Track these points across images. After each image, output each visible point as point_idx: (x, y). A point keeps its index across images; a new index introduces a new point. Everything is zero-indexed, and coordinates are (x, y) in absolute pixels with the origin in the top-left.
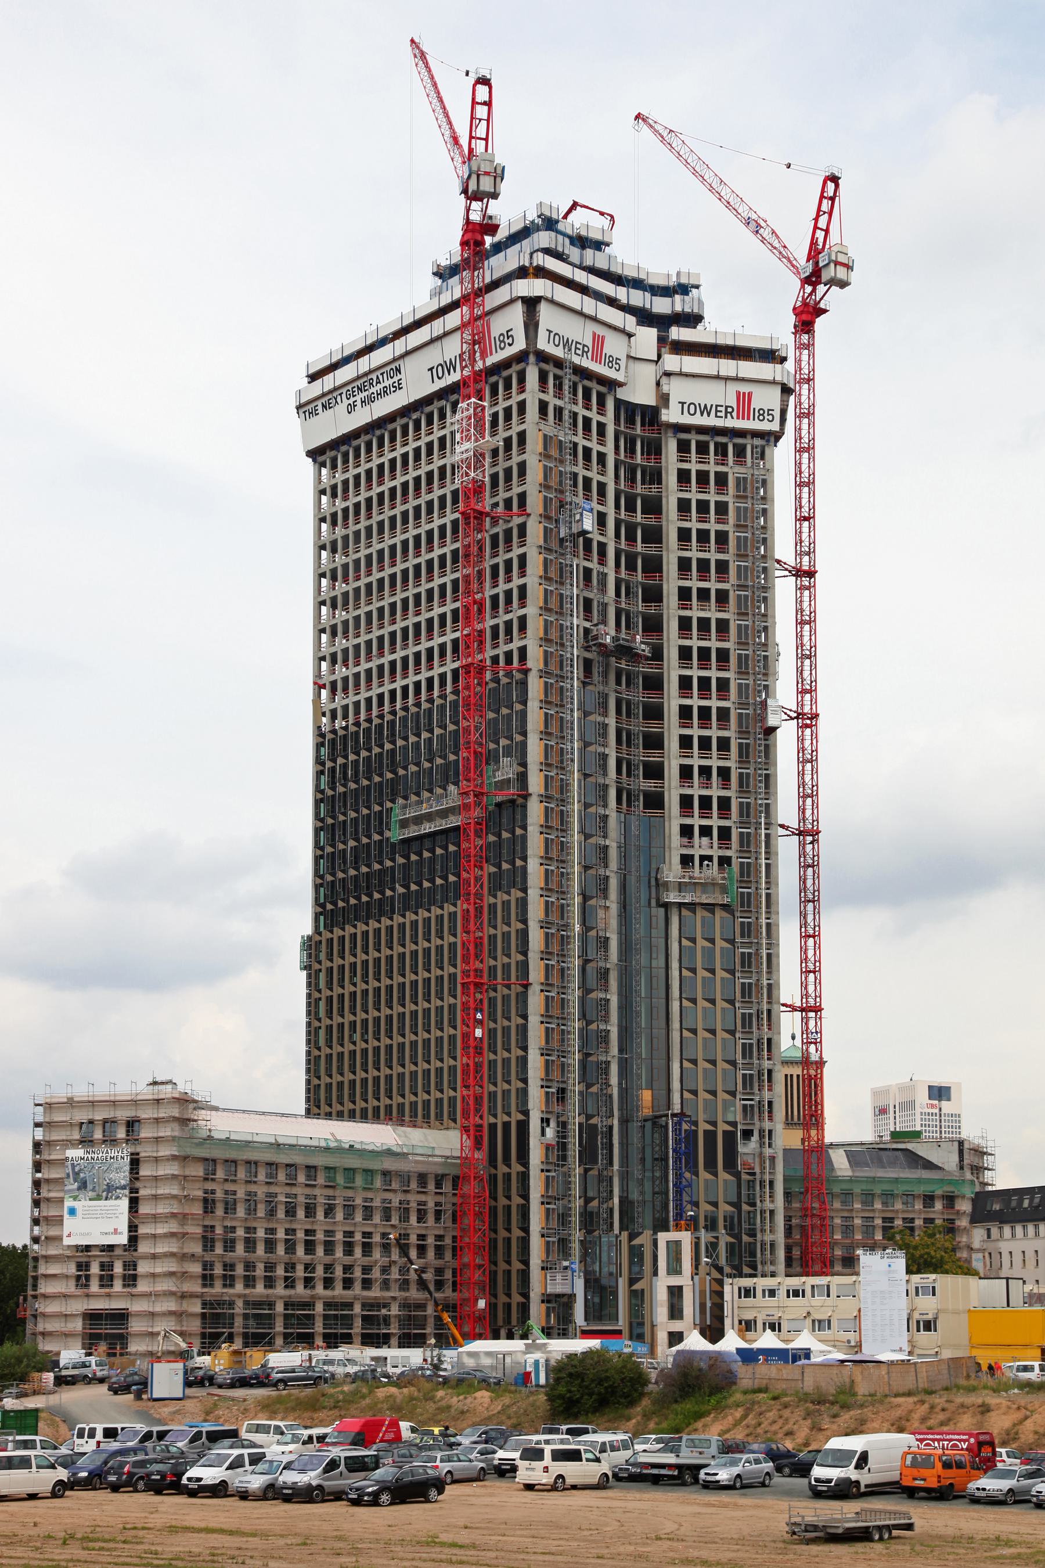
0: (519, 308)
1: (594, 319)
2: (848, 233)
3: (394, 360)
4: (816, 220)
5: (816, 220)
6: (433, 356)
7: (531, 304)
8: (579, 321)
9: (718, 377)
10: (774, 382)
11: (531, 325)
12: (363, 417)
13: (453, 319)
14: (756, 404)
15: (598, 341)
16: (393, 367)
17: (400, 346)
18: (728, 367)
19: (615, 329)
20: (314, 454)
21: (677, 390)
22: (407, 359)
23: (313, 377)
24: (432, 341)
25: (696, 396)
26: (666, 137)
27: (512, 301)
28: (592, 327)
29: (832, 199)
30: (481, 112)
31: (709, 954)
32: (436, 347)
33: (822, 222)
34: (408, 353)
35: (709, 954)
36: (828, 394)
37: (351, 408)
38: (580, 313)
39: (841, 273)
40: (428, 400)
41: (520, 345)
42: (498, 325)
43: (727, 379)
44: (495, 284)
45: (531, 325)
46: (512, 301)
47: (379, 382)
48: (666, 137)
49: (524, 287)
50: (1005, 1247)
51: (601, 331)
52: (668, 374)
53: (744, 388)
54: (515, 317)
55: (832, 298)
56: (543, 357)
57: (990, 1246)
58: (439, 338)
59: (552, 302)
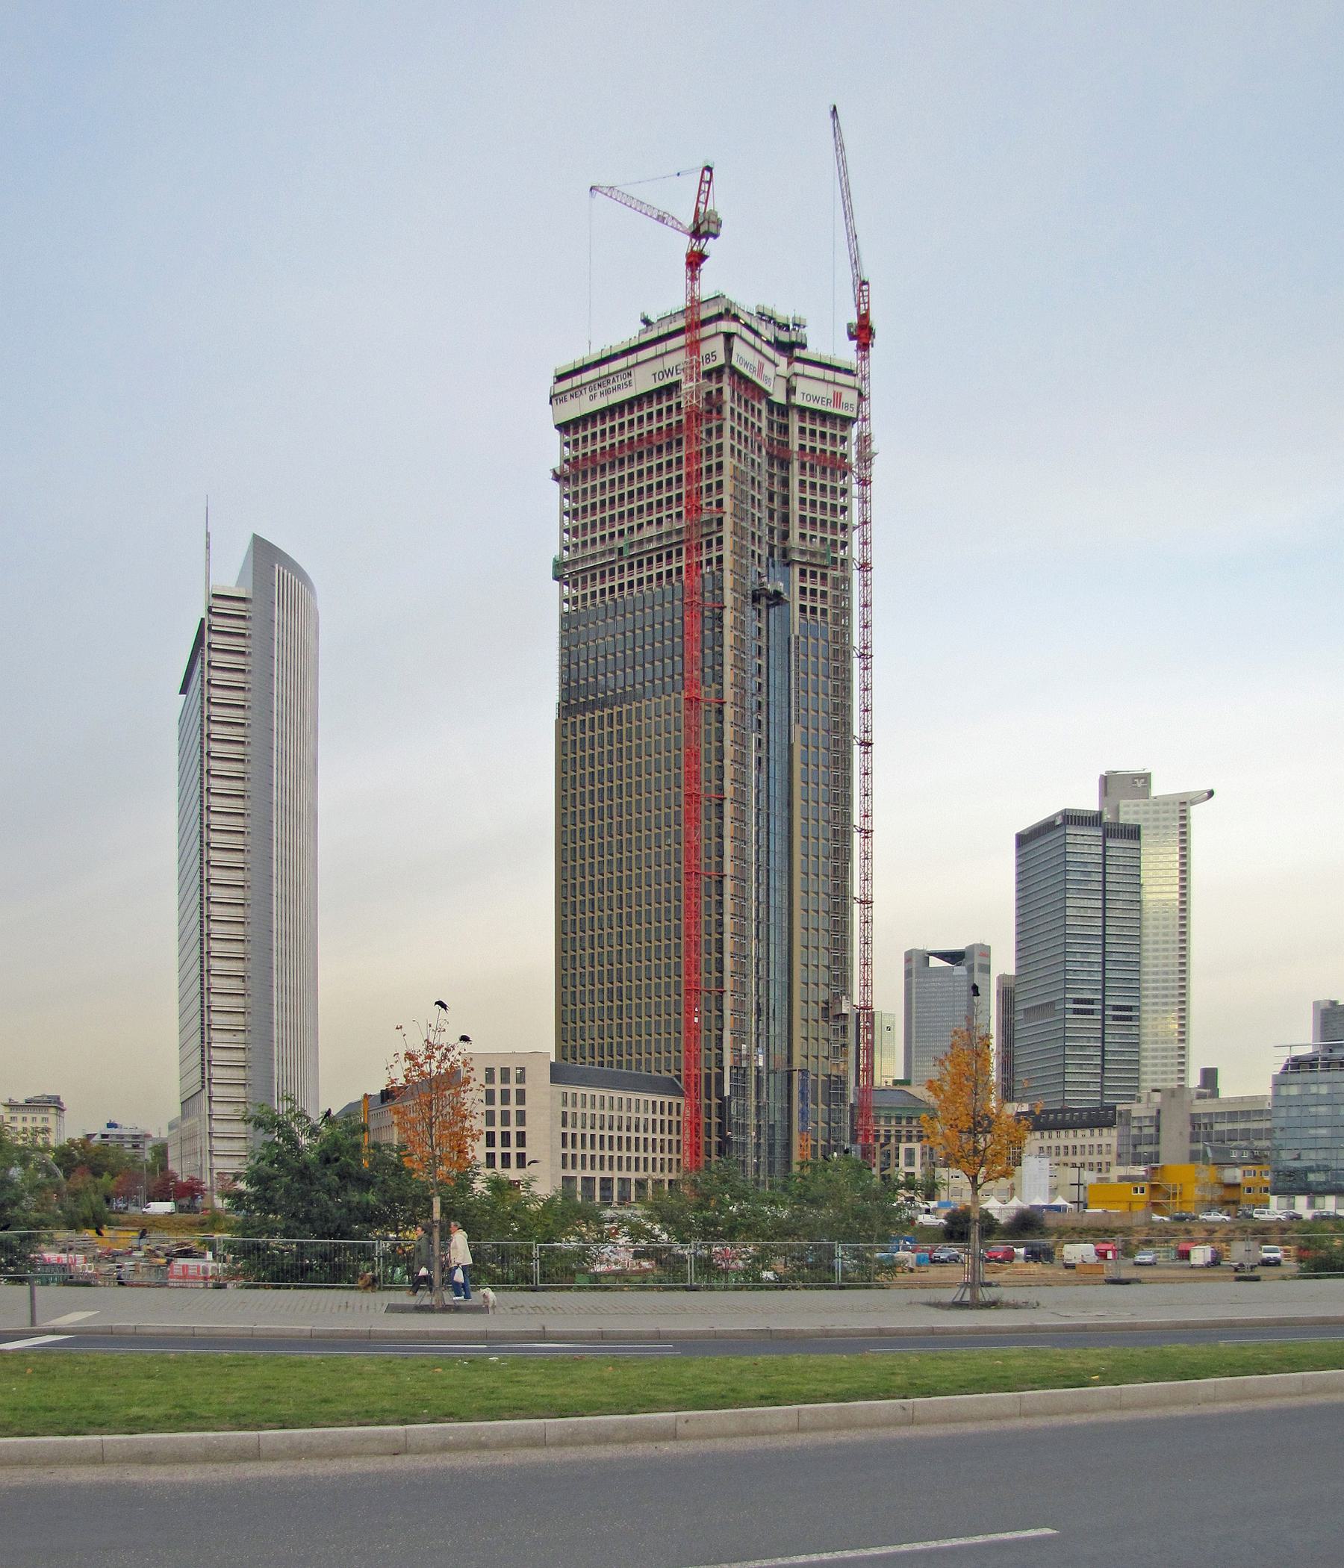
0: (721, 338)
1: (834, 383)
2: (719, 204)
3: (628, 368)
6: (657, 366)
7: (729, 337)
8: (824, 385)
9: (823, 380)
10: (854, 388)
11: (729, 351)
13: (680, 341)
14: (844, 399)
15: (761, 366)
16: (628, 370)
17: (631, 359)
18: (829, 375)
19: (849, 387)
20: (563, 427)
21: (801, 385)
23: (560, 378)
24: (657, 357)
25: (811, 392)
27: (717, 334)
28: (832, 388)
29: (709, 183)
31: (816, 665)
32: (659, 361)
33: (702, 198)
34: (638, 364)
35: (816, 665)
36: (876, 389)
37: (593, 397)
38: (823, 380)
39: (713, 229)
40: (648, 396)
41: (721, 360)
42: (705, 349)
43: (828, 382)
44: (705, 323)
45: (729, 351)
46: (717, 334)
49: (725, 326)
52: (796, 375)
53: (838, 389)
54: (719, 344)
55: (710, 246)
56: (734, 371)
58: (662, 355)
59: (740, 337)
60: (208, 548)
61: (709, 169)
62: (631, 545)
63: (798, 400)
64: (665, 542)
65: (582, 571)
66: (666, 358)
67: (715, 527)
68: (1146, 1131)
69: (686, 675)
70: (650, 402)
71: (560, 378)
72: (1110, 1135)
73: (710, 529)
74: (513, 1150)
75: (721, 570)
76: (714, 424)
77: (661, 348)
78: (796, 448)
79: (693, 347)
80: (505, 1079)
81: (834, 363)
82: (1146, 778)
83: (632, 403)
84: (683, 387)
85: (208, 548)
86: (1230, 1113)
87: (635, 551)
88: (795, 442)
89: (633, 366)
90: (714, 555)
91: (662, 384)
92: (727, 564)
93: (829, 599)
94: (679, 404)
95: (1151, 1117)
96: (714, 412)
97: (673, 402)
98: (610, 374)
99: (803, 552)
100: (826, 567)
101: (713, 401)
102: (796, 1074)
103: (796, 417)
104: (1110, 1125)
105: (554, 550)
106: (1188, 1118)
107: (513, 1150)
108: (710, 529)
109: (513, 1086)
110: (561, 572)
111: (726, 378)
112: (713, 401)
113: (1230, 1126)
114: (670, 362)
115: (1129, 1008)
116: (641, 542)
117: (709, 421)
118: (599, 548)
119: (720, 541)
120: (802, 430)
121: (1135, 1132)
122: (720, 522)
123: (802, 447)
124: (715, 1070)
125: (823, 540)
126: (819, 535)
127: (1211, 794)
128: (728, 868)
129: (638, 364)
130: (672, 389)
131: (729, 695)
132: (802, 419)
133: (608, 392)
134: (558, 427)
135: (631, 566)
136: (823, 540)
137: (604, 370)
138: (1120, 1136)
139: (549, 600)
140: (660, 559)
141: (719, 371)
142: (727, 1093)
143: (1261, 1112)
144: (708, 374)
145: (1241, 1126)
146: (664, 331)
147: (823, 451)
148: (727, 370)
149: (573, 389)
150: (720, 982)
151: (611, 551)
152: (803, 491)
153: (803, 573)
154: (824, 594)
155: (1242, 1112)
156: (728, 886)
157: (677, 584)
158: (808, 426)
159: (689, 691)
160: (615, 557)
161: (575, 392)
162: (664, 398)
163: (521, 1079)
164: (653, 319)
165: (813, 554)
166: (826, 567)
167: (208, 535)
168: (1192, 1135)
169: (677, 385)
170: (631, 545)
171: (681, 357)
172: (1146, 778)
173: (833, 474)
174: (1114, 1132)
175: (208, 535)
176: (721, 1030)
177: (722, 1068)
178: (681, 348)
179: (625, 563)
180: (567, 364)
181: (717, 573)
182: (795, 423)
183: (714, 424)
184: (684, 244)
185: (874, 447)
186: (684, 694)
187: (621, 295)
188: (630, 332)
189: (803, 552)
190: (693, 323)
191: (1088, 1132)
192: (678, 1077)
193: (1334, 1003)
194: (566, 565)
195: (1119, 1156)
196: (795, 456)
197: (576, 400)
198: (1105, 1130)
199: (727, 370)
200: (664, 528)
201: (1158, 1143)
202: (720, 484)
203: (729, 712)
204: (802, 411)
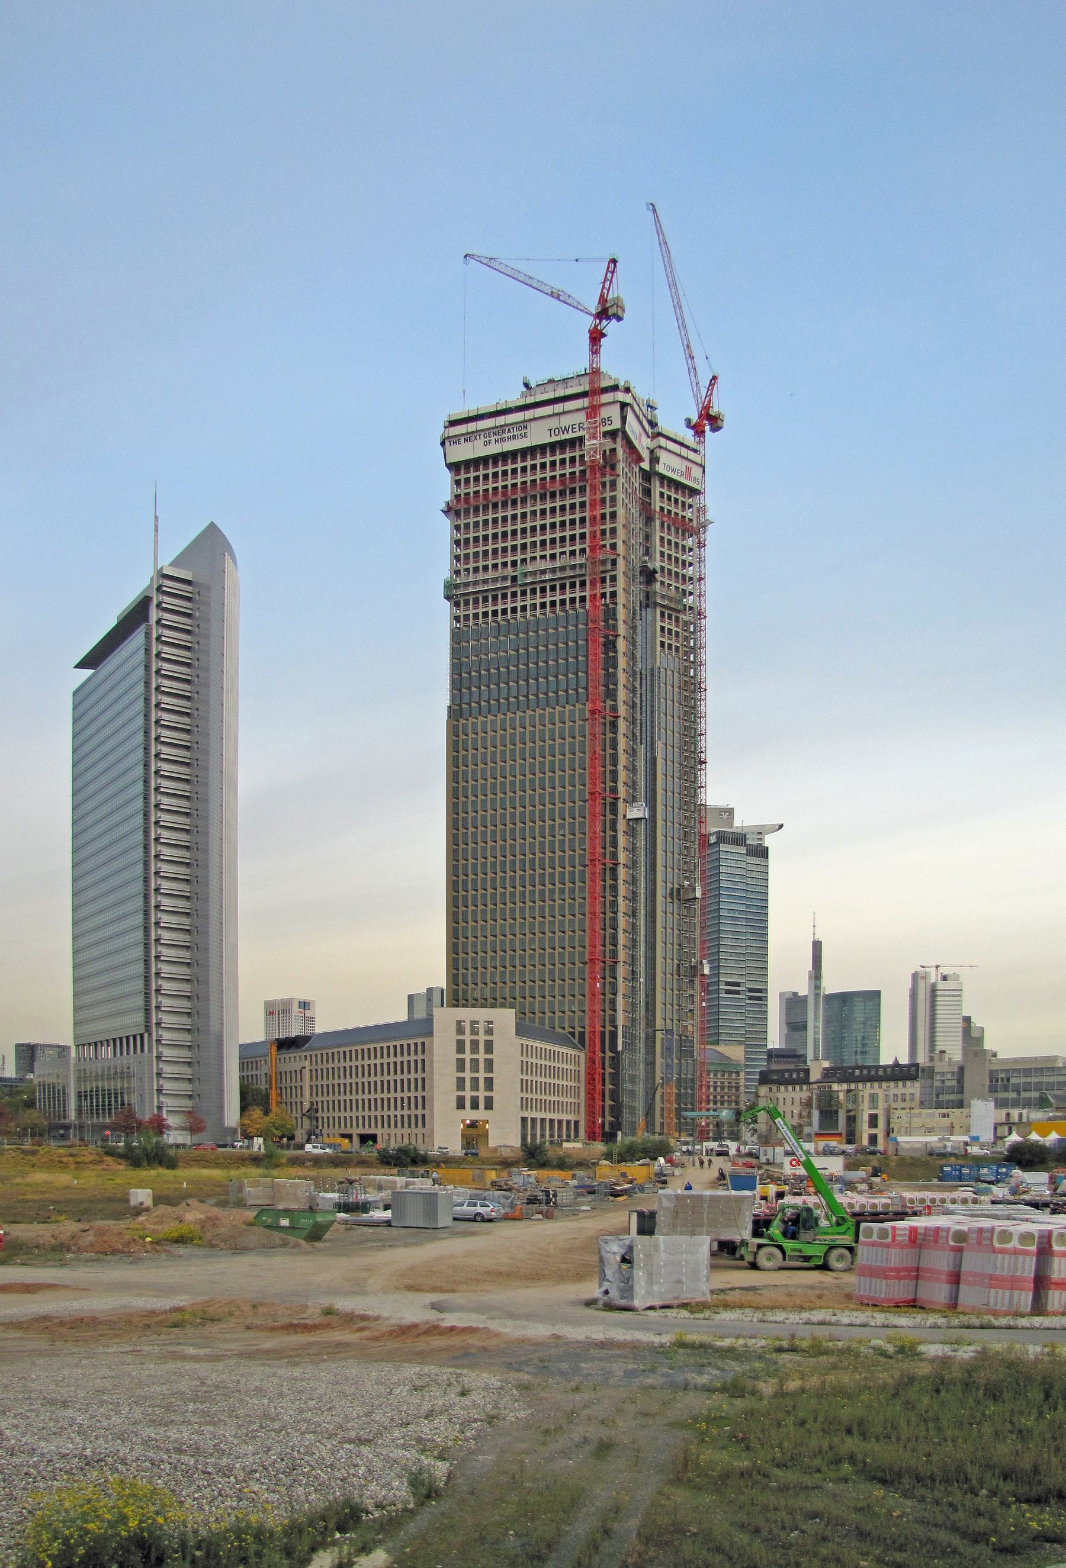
0: (618, 406)
1: (687, 459)
2: (621, 290)
3: (525, 421)
4: (604, 283)
5: (604, 283)
6: (554, 423)
7: (624, 406)
8: (680, 459)
9: (680, 455)
11: (624, 419)
12: (495, 449)
13: (585, 402)
15: (689, 470)
17: (528, 414)
20: (454, 467)
21: (663, 456)
22: (533, 424)
23: (453, 423)
24: (554, 415)
26: (489, 263)
27: (614, 402)
28: (686, 463)
29: (613, 272)
30: (609, 276)
33: (607, 284)
34: (535, 419)
37: (487, 443)
38: (680, 455)
40: (542, 448)
41: (616, 425)
42: (604, 413)
43: (683, 457)
46: (614, 402)
47: (509, 431)
48: (489, 263)
49: (621, 396)
50: (781, 1096)
51: (690, 465)
52: (660, 447)
54: (615, 412)
55: (611, 327)
57: (772, 1095)
58: (559, 414)
60: (156, 531)
61: (614, 261)
62: (525, 575)
63: (660, 469)
64: (559, 575)
65: (465, 594)
66: (563, 418)
67: (609, 566)
68: (948, 1083)
69: (590, 689)
70: (543, 454)
71: (453, 423)
72: (913, 1087)
73: (572, 571)
74: (482, 1094)
75: (616, 604)
76: (608, 479)
77: (559, 408)
78: (658, 509)
79: (592, 411)
80: (474, 1031)
81: (686, 443)
82: (730, 812)
83: (524, 453)
84: (587, 443)
85: (156, 531)
86: (1025, 1070)
87: (529, 580)
88: (657, 504)
89: (530, 420)
90: (608, 590)
91: (558, 439)
92: (621, 598)
93: (681, 638)
94: (582, 456)
95: (953, 1073)
96: (608, 469)
97: (577, 454)
98: (506, 425)
99: (663, 597)
100: (679, 611)
101: (609, 461)
102: (659, 1035)
103: (658, 483)
104: (914, 1078)
105: (446, 574)
106: (987, 1073)
107: (482, 1094)
108: (572, 571)
109: (482, 1038)
110: (453, 594)
111: (619, 440)
112: (609, 461)
113: (1023, 1080)
114: (566, 421)
115: (760, 991)
116: (534, 573)
117: (603, 475)
118: (491, 574)
119: (614, 579)
120: (662, 495)
121: (937, 1084)
122: (614, 562)
123: (662, 509)
124: (609, 1028)
125: (677, 588)
126: (675, 584)
127: (781, 826)
128: (622, 857)
129: (535, 419)
130: (573, 443)
131: (622, 710)
132: (662, 486)
133: (502, 440)
134: (450, 466)
135: (524, 593)
136: (677, 588)
137: (501, 420)
138: (921, 1087)
139: (441, 616)
140: (573, 585)
141: (612, 434)
142: (620, 1048)
143: (1053, 1069)
144: (605, 434)
145: (1034, 1080)
146: (540, 398)
147: (676, 514)
148: (620, 434)
149: (467, 433)
150: (614, 954)
151: (504, 578)
152: (662, 546)
153: (662, 614)
154: (677, 633)
155: (1036, 1069)
156: (622, 873)
157: (581, 611)
158: (666, 493)
159: (594, 703)
160: (509, 583)
161: (469, 437)
162: (558, 452)
163: (489, 1032)
164: (533, 385)
165: (670, 599)
166: (679, 611)
167: (156, 518)
168: (990, 1086)
169: (581, 440)
170: (525, 575)
171: (581, 417)
172: (730, 812)
173: (683, 535)
174: (917, 1084)
175: (156, 518)
176: (615, 994)
177: (616, 1027)
178: (584, 409)
179: (518, 590)
180: (459, 412)
181: (611, 606)
182: (657, 488)
183: (608, 479)
184: (588, 322)
185: (709, 516)
186: (589, 706)
187: (513, 356)
188: (514, 396)
189: (663, 597)
190: (595, 390)
191: (892, 1084)
192: (573, 1034)
193: (795, 994)
194: (457, 586)
195: (922, 1103)
196: (657, 516)
197: (469, 444)
198: (908, 1083)
199: (620, 434)
200: (558, 564)
201: (962, 1092)
202: (613, 531)
203: (622, 726)
204: (662, 478)
